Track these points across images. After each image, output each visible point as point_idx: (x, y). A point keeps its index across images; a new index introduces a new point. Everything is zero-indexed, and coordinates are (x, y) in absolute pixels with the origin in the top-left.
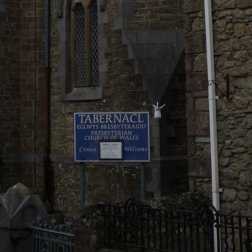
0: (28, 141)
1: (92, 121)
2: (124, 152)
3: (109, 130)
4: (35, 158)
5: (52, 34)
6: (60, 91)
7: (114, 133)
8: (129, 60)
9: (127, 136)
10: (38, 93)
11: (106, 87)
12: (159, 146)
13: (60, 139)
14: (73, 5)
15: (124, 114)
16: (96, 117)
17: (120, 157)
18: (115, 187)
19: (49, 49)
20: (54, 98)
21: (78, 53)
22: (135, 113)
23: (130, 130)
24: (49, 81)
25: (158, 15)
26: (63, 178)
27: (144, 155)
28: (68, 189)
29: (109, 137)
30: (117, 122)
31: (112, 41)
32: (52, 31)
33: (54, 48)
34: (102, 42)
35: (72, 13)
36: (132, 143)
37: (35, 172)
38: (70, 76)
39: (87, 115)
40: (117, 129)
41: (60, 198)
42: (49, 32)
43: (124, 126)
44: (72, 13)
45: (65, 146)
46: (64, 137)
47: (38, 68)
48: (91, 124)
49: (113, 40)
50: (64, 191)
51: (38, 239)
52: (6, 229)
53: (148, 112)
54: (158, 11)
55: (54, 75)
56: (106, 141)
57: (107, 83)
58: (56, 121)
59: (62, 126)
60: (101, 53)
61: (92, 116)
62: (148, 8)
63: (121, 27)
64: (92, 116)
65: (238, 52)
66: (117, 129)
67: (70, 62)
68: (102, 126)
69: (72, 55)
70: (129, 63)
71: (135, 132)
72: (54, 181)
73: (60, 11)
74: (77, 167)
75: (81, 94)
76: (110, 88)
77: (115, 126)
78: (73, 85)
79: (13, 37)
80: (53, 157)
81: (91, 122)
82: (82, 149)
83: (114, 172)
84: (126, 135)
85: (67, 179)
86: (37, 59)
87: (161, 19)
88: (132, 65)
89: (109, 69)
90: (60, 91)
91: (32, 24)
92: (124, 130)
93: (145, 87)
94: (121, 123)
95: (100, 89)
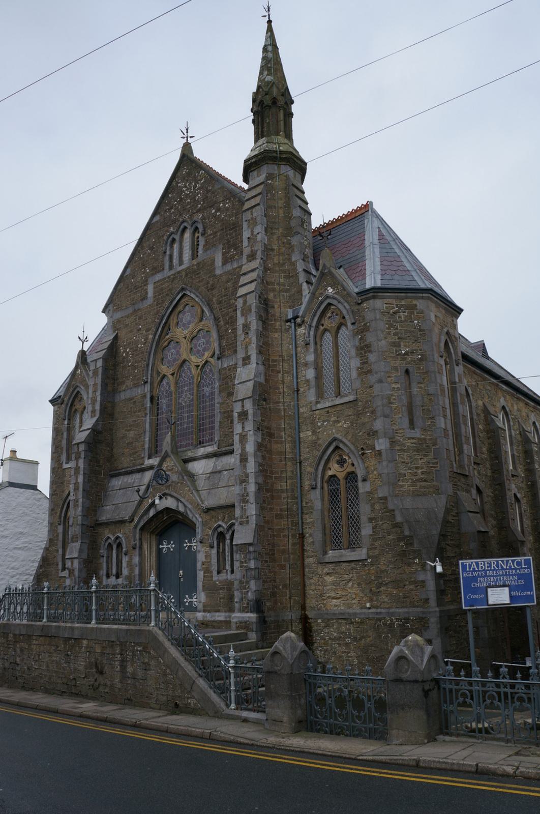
1: (478, 568)
2: (511, 597)
3: (495, 576)
4: (292, 615)
5: (304, 504)
6: (315, 554)
7: (500, 579)
8: (397, 523)
9: (512, 580)
10: (292, 556)
11: (371, 549)
12: (435, 598)
13: (317, 598)
14: (326, 477)
15: (509, 560)
16: (481, 564)
17: (508, 602)
18: (386, 637)
19: (302, 517)
20: (309, 561)
21: (333, 520)
22: (518, 559)
23: (515, 575)
24: (303, 545)
25: (418, 483)
27: (530, 598)
28: (330, 642)
29: (496, 583)
30: (503, 569)
31: (376, 507)
32: (304, 500)
33: (307, 516)
34: (365, 510)
35: (325, 485)
36: (517, 588)
38: (325, 541)
39: (472, 563)
40: (503, 575)
41: (321, 651)
42: (302, 502)
43: (509, 572)
44: (325, 485)
45: (323, 604)
46: (321, 595)
47: (290, 534)
48: (476, 571)
49: (377, 506)
50: (324, 644)
51: (451, 691)
52: (416, 681)
53: (531, 558)
54: (418, 481)
55: (309, 540)
56: (493, 587)
57: (372, 544)
58: (312, 581)
59: (319, 585)
60: (364, 519)
61: (477, 564)
62: (409, 477)
63: (386, 494)
64: (477, 564)
66: (503, 575)
67: (325, 527)
68: (488, 572)
69: (326, 522)
70: (397, 525)
71: (520, 577)
72: (312, 635)
73: (314, 483)
74: (340, 621)
75: (341, 556)
76: (375, 548)
77: (501, 572)
78: (328, 548)
79: (269, 506)
80: (310, 614)
81: (476, 569)
82: (470, 597)
83: (385, 624)
84: (512, 580)
85: (328, 633)
87: (421, 487)
88: (400, 527)
89: (373, 532)
90: (315, 554)
91: (284, 495)
92: (510, 575)
93: (416, 546)
94: (507, 569)
95: (364, 551)
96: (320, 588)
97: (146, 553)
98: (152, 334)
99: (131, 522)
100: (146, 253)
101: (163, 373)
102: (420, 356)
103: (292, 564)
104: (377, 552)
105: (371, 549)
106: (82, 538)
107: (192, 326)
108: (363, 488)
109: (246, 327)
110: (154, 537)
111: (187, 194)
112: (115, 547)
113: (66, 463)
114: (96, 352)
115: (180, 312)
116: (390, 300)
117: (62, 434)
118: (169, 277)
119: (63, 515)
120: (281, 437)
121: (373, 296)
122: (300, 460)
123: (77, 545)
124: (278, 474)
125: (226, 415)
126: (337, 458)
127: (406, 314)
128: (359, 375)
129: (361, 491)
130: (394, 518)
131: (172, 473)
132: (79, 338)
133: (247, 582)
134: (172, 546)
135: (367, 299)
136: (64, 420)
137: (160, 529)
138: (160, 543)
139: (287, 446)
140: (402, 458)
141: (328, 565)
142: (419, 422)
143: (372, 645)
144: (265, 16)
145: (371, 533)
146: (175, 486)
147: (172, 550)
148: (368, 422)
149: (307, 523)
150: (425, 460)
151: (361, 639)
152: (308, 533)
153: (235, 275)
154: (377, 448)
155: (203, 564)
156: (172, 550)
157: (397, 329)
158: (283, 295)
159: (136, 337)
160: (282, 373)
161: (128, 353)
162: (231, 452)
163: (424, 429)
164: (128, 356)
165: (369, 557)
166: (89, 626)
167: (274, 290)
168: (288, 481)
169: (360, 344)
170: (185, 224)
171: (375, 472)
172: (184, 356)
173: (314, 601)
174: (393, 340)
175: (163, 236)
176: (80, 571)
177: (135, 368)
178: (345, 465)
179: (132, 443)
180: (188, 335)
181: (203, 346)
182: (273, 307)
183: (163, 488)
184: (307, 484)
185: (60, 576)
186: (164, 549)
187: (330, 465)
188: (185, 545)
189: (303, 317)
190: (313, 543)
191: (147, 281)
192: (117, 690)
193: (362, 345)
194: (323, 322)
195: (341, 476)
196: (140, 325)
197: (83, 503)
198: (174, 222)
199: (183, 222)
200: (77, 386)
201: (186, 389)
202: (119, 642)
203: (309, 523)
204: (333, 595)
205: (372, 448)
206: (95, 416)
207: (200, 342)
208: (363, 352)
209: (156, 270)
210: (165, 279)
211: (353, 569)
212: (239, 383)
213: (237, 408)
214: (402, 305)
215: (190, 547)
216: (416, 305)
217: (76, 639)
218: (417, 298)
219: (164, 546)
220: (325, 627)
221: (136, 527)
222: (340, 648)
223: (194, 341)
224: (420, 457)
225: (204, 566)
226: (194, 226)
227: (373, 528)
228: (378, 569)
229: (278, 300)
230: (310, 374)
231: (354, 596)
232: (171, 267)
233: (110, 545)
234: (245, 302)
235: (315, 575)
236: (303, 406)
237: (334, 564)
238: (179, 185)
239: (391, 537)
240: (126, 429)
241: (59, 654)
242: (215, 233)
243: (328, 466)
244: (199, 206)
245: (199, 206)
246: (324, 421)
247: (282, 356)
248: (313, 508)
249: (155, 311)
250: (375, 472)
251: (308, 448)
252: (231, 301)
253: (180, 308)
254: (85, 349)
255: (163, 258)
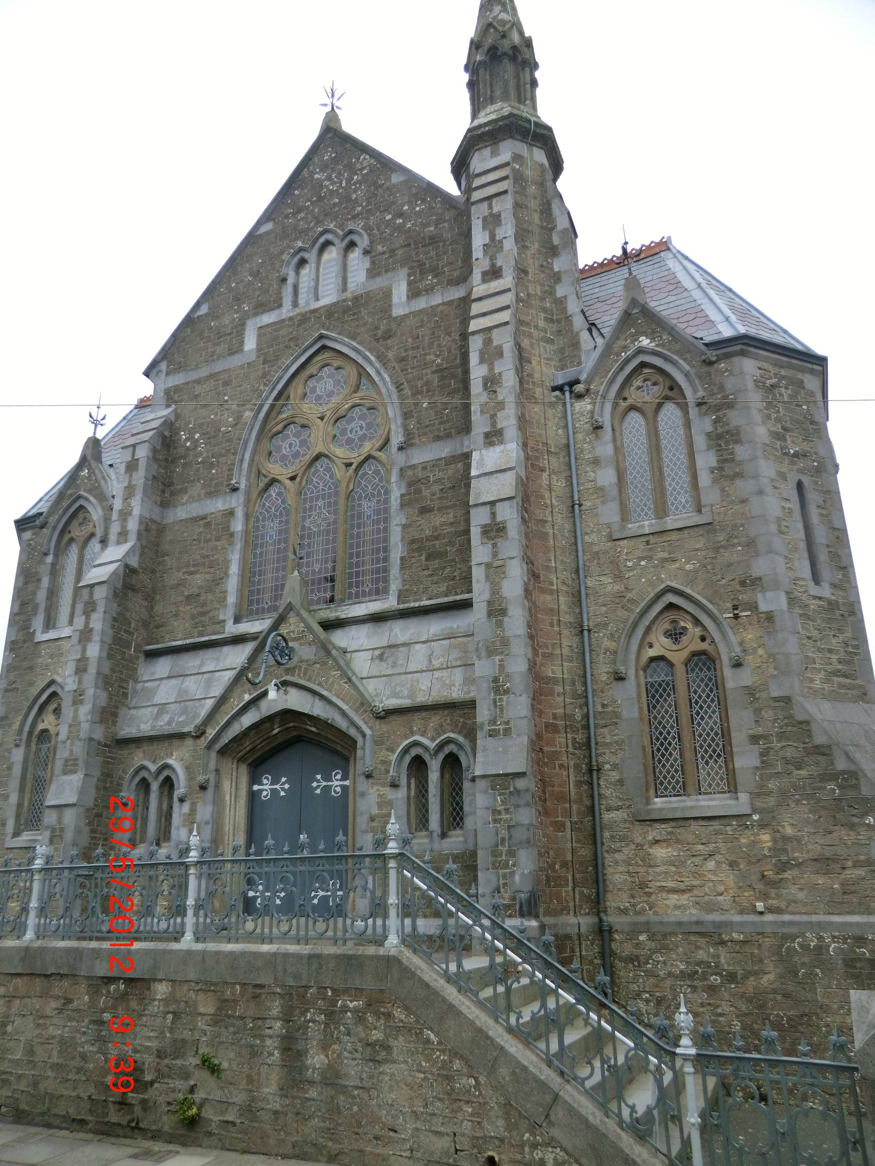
0: (564, 894)
8: (817, 747)
10: (575, 807)
25: (835, 679)
26: (651, 961)
33: (606, 730)
37: (581, 951)
41: (647, 1001)
44: (641, 673)
49: (767, 714)
59: (637, 864)
65: (172, 1010)
80: (611, 919)
83: (805, 947)
85: (664, 963)
86: (571, 749)
87: (841, 686)
89: (763, 762)
90: (627, 803)
91: (559, 689)
96: (641, 870)
97: (228, 798)
98: (251, 410)
99: (197, 737)
100: (242, 281)
101: (271, 476)
102: (815, 464)
103: (576, 823)
104: (771, 802)
105: (759, 795)
106: (87, 764)
107: (335, 400)
108: (732, 680)
109: (491, 383)
110: (244, 769)
111: (332, 191)
112: (155, 786)
113: (43, 632)
114: (142, 423)
115: (311, 376)
116: (764, 364)
117: (39, 580)
118: (291, 319)
119: (27, 728)
120: (552, 584)
121: (742, 350)
122: (588, 626)
123: (76, 779)
124: (547, 647)
125: (415, 546)
126: (667, 626)
127: (789, 392)
128: (715, 481)
129: (730, 685)
130: (810, 736)
131: (301, 644)
132: (91, 416)
133: (512, 853)
134: (283, 786)
135: (728, 356)
136: (46, 554)
137: (258, 754)
138: (254, 779)
139: (562, 599)
140: (807, 629)
141: (657, 825)
142: (826, 574)
143: (775, 991)
144: (325, 105)
145: (757, 763)
146: (306, 669)
147: (282, 794)
148: (739, 562)
149: (606, 744)
150: (841, 639)
151: (745, 977)
152: (608, 763)
153: (436, 315)
154: (763, 607)
155: (372, 819)
156: (282, 794)
157: (778, 412)
158: (545, 347)
159: (216, 415)
160: (547, 473)
161: (197, 440)
162: (466, 605)
163: (834, 586)
164: (196, 447)
165: (755, 811)
166: (175, 946)
167: (530, 336)
168: (565, 664)
169: (716, 428)
170: (329, 237)
171: (761, 651)
172: (320, 448)
173: (625, 896)
174: (775, 429)
175: (282, 253)
176: (78, 831)
177: (212, 465)
178: (685, 639)
179: (198, 595)
180: (328, 414)
181: (360, 433)
182: (530, 362)
183: (281, 670)
184: (603, 671)
185: (6, 846)
186: (264, 793)
187: (652, 638)
188: (315, 784)
189: (588, 382)
190: (621, 782)
191: (244, 324)
192: (265, 1116)
193: (720, 430)
194: (626, 394)
195: (678, 658)
196: (225, 395)
197: (95, 697)
198: (305, 232)
199: (326, 231)
200: (80, 497)
201: (320, 503)
202: (283, 986)
203: (611, 744)
204: (670, 884)
205: (753, 607)
206: (126, 541)
207: (353, 425)
208: (721, 442)
209: (261, 308)
210: (283, 321)
211: (717, 833)
212: (479, 476)
213: (479, 518)
214: (784, 377)
215: (326, 789)
216: (802, 382)
217: (131, 980)
218: (803, 370)
219: (265, 787)
220: (654, 951)
221: (209, 747)
222: (695, 995)
223: (340, 424)
224: (832, 633)
225: (374, 824)
226: (347, 240)
227: (762, 755)
228: (778, 835)
229: (537, 354)
230: (606, 477)
231: (721, 888)
232: (295, 304)
233: (145, 785)
234: (488, 341)
235: (627, 845)
236: (592, 532)
237: (673, 824)
238: (316, 176)
239: (804, 773)
240: (184, 570)
241: (71, 1019)
242: (392, 251)
243: (648, 640)
244: (359, 208)
245: (359, 208)
246: (641, 559)
247: (547, 444)
248: (617, 715)
249: (260, 373)
250: (761, 651)
251: (604, 605)
252: (428, 358)
253: (312, 369)
254: (99, 436)
255: (280, 288)
